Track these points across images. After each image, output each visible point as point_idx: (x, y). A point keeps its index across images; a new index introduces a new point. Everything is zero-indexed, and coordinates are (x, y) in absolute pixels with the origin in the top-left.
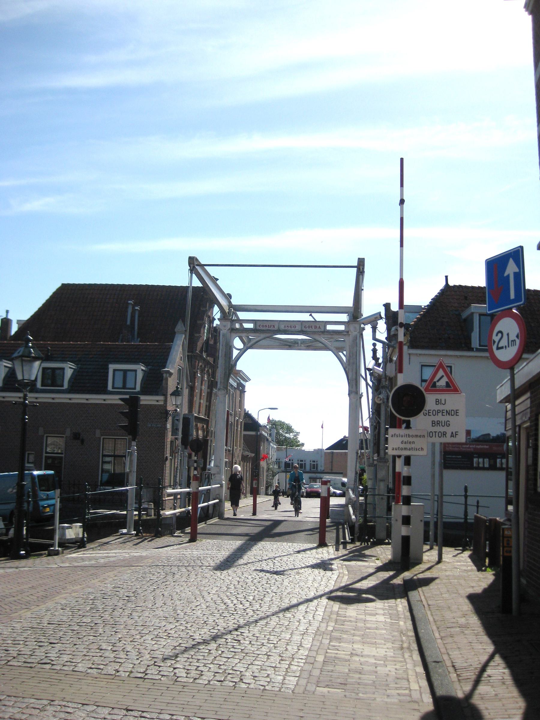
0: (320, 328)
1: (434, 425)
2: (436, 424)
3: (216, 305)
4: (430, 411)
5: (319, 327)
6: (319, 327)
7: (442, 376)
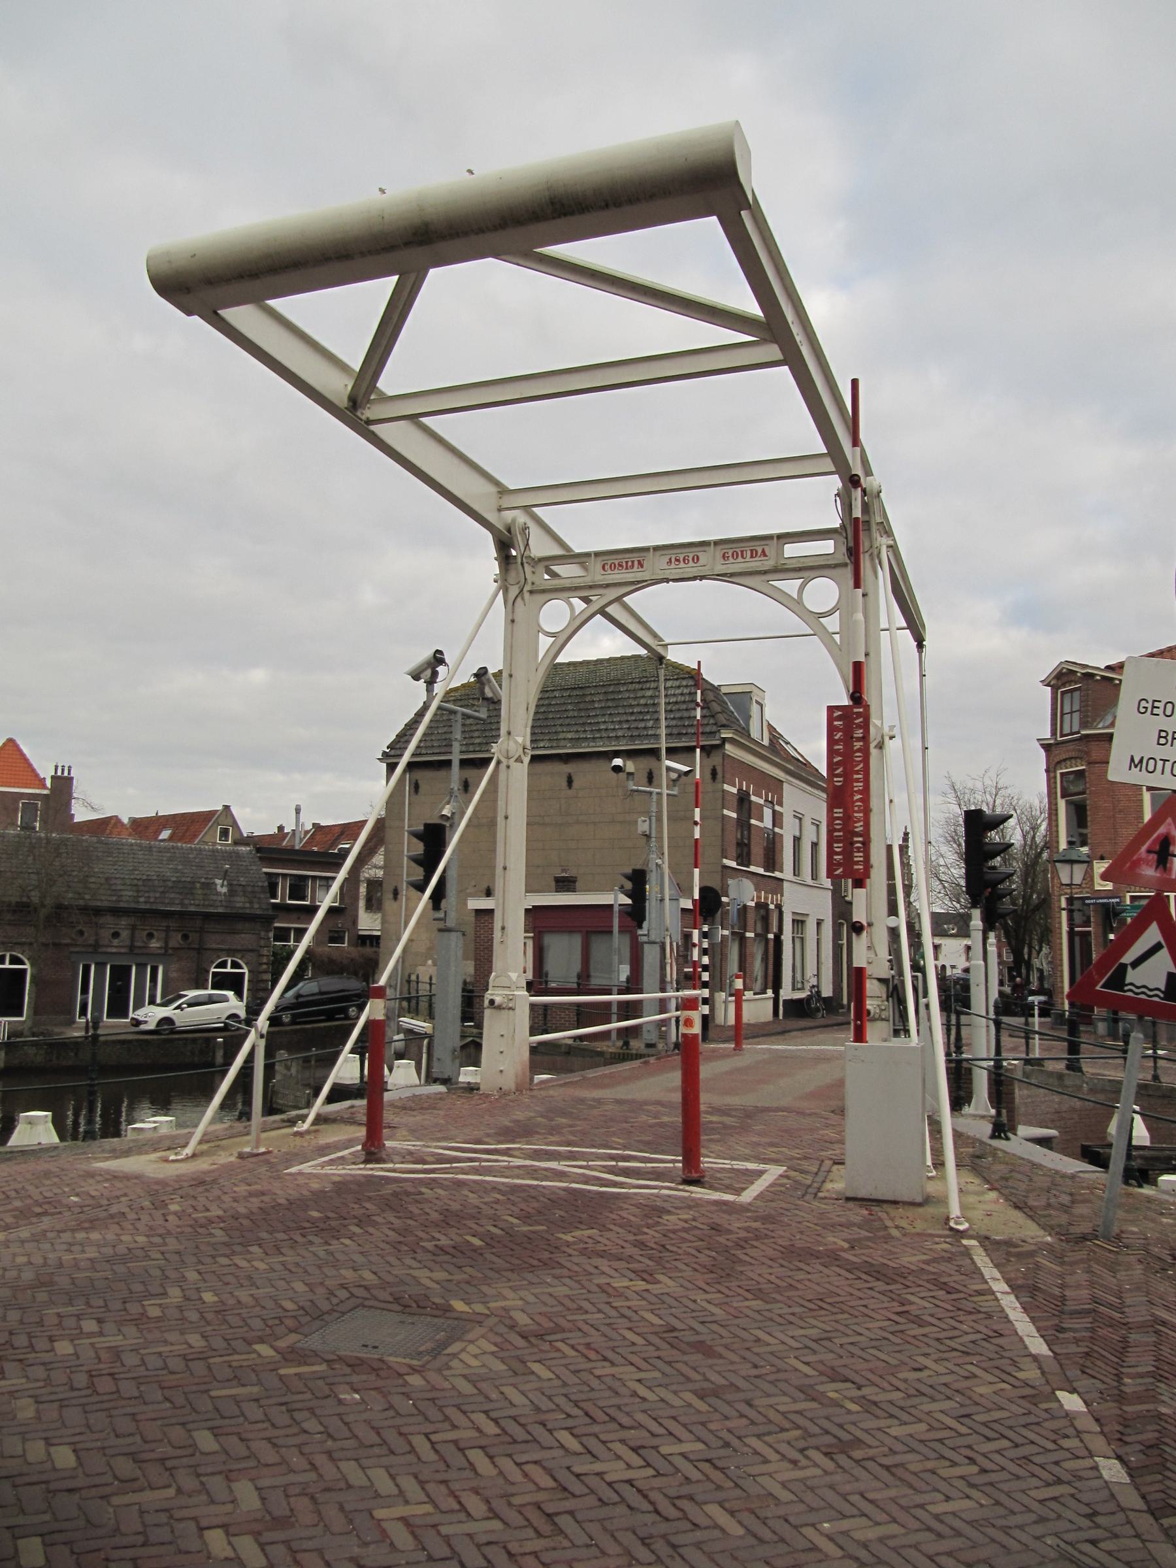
0: (765, 555)
1: (1163, 741)
2: (1169, 738)
3: (396, 278)
4: (1156, 704)
5: (763, 551)
6: (763, 551)
7: (1157, 948)
